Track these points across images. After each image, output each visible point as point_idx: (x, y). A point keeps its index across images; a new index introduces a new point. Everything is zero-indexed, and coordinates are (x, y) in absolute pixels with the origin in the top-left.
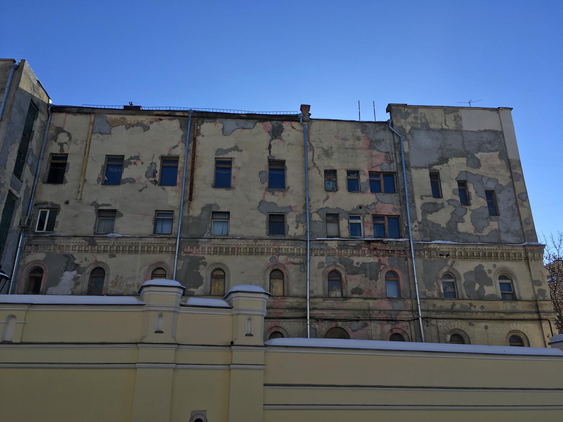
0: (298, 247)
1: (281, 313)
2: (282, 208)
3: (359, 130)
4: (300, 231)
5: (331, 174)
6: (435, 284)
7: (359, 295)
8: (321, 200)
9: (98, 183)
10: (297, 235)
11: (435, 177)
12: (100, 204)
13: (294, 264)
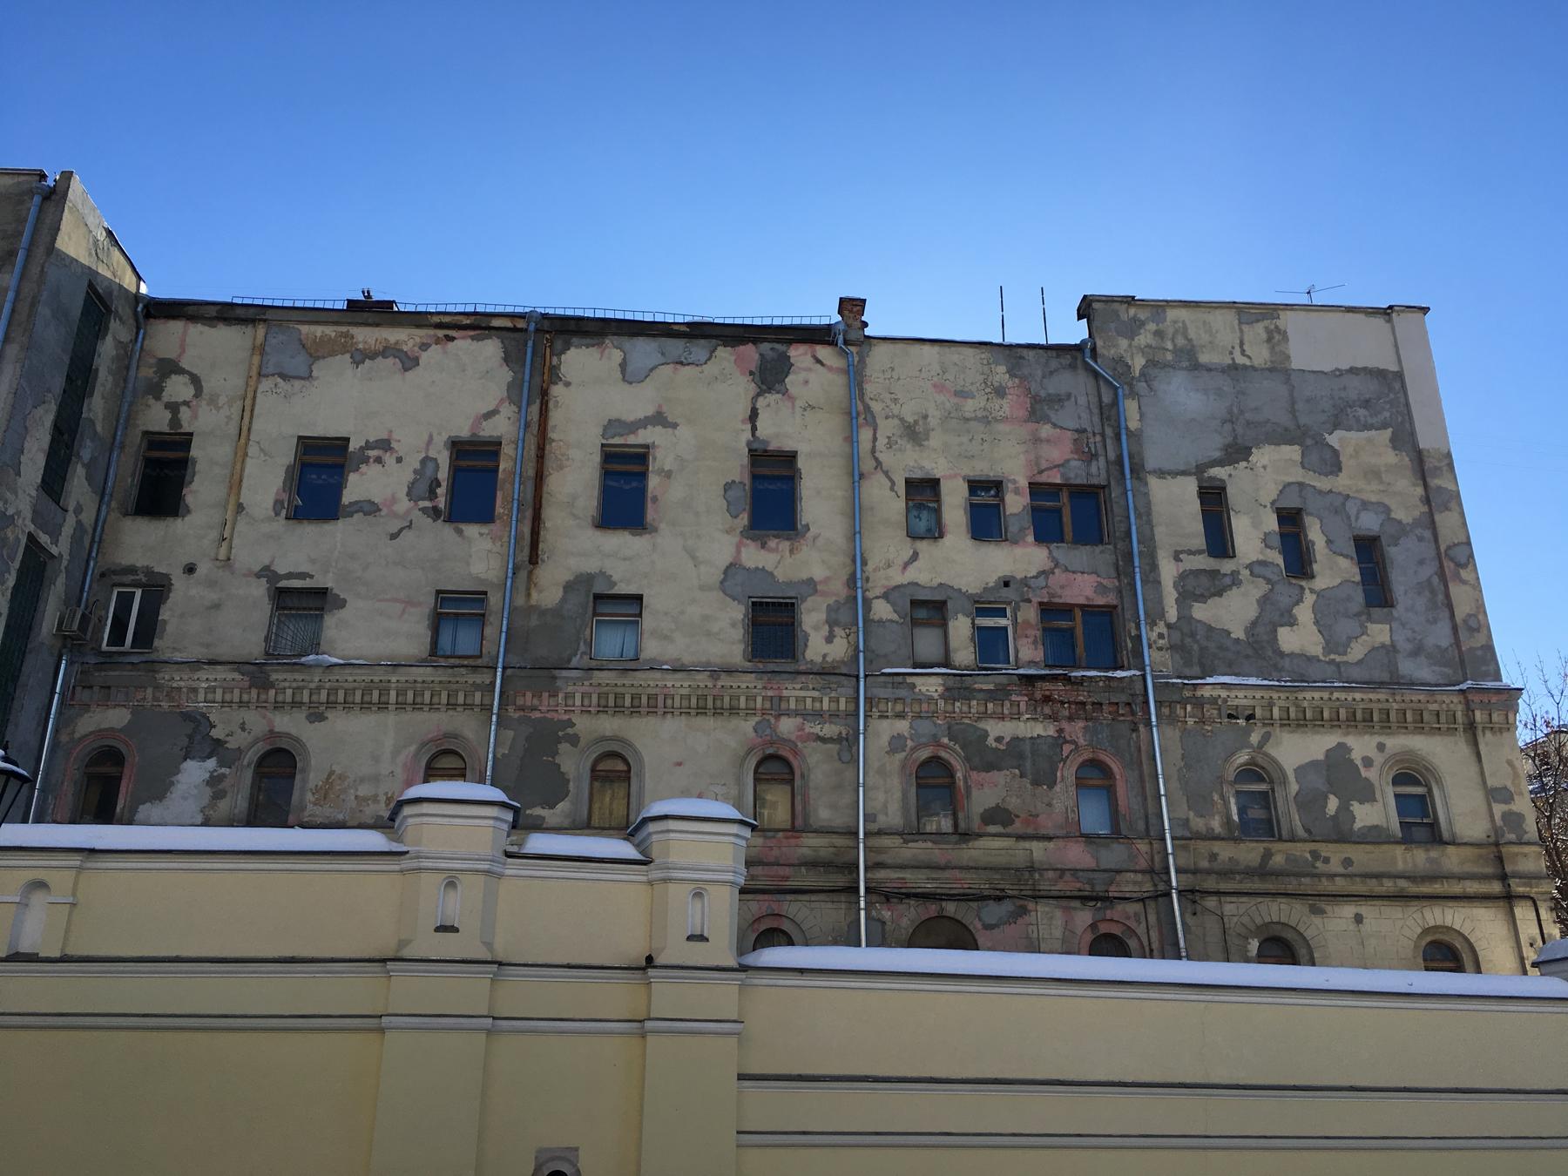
1: (786, 878)
3: (1002, 369)
9: (277, 514)
12: (282, 571)
13: (823, 740)
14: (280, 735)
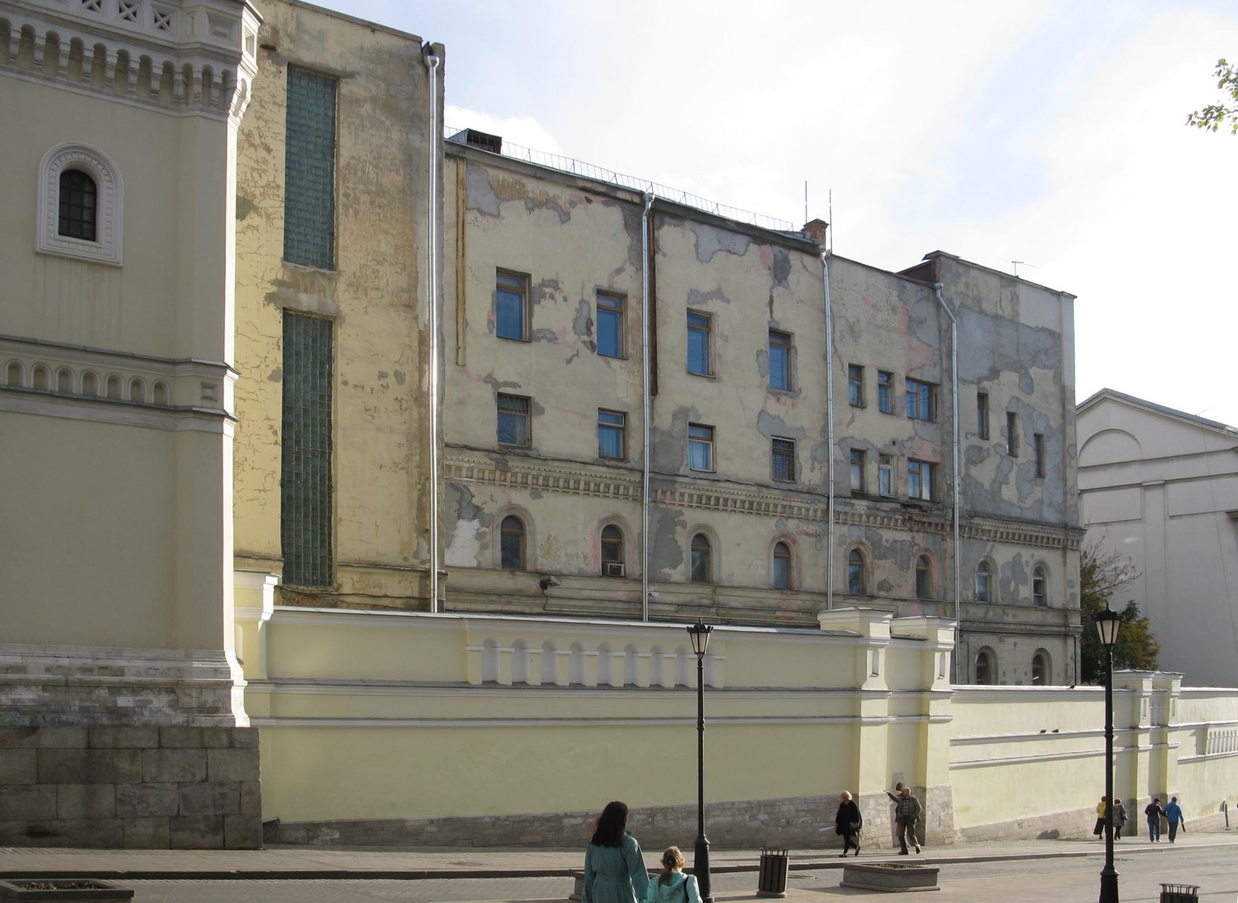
1: (791, 618)
3: (895, 293)
9: (491, 332)
11: (982, 398)
12: (501, 380)
13: (808, 534)
14: (514, 507)
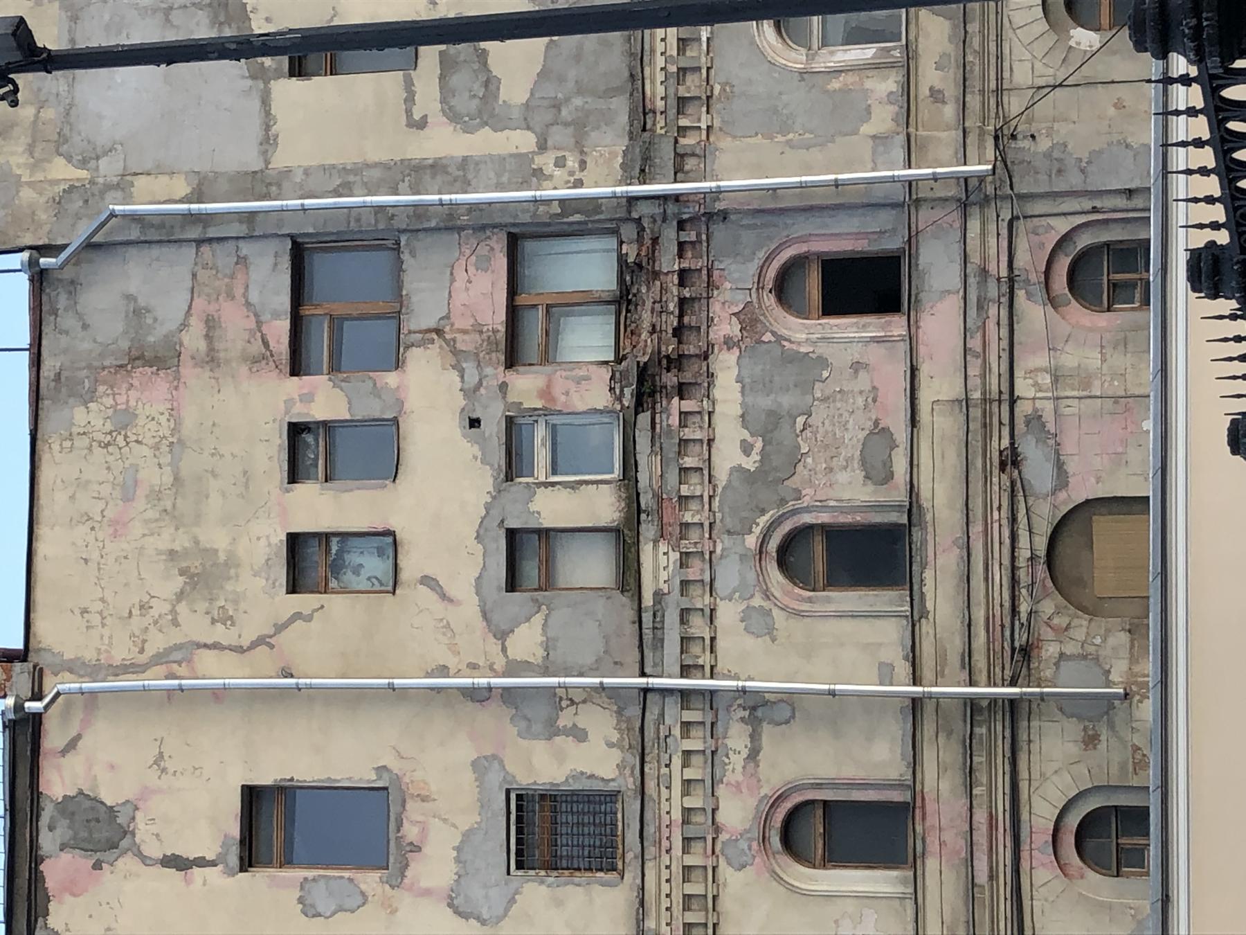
0: (677, 731)
1: (992, 819)
2: (483, 805)
3: (80, 415)
4: (601, 725)
5: (307, 561)
6: (835, 84)
7: (893, 446)
8: (441, 616)
10: (615, 736)
13: (753, 755)
